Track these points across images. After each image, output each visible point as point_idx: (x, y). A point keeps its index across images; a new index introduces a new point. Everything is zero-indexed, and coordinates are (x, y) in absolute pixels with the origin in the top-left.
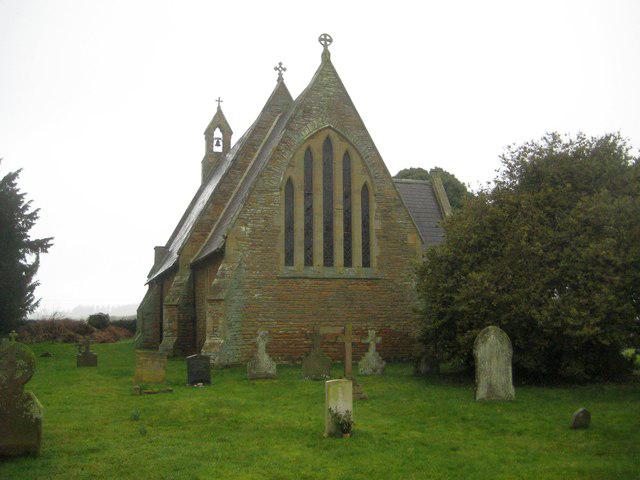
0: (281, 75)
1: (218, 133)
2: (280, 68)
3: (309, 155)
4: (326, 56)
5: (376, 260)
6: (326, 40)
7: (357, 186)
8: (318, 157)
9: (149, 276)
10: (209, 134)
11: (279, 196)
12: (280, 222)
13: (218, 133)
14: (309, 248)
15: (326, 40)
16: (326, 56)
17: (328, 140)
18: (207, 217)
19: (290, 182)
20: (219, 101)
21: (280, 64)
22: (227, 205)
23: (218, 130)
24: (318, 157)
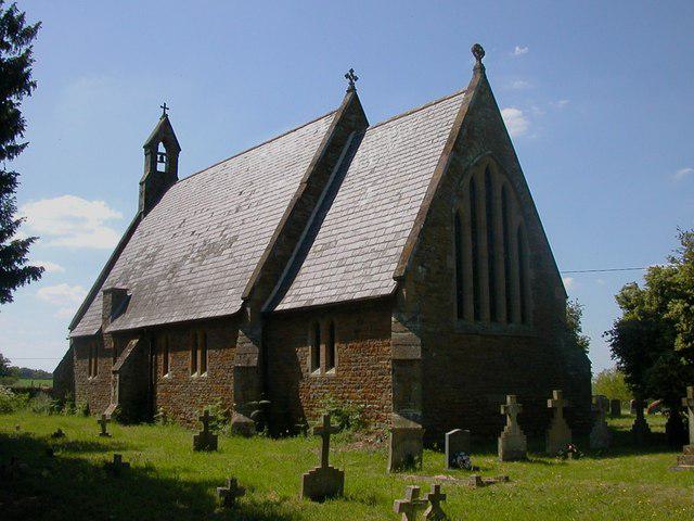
0: (352, 84)
1: (162, 148)
2: (351, 77)
3: (473, 185)
4: (352, 89)
5: (532, 315)
6: (351, 77)
7: (513, 230)
8: (481, 186)
9: (72, 328)
10: (151, 148)
11: (450, 229)
12: (451, 263)
13: (162, 148)
14: (509, 311)
15: (478, 52)
16: (352, 89)
17: (487, 170)
18: (278, 253)
19: (458, 218)
20: (165, 108)
21: (352, 71)
22: (303, 237)
23: (161, 144)
24: (481, 186)
